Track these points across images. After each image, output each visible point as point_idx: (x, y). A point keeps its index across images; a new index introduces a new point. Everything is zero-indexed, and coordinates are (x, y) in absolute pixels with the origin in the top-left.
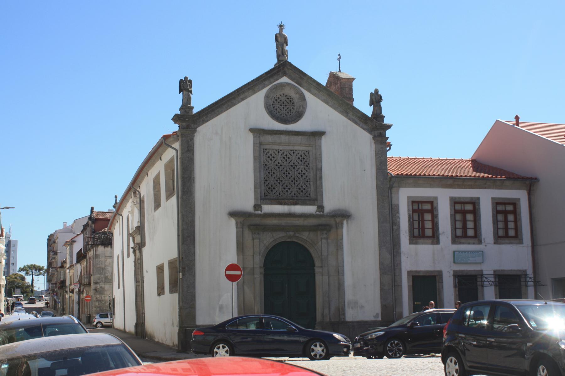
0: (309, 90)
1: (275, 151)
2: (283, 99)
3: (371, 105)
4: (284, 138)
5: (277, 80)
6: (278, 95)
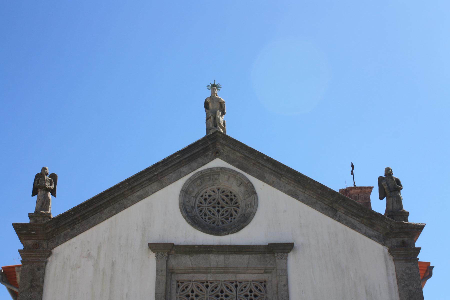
1: (200, 285)
2: (218, 196)
3: (381, 198)
4: (215, 260)
5: (204, 164)
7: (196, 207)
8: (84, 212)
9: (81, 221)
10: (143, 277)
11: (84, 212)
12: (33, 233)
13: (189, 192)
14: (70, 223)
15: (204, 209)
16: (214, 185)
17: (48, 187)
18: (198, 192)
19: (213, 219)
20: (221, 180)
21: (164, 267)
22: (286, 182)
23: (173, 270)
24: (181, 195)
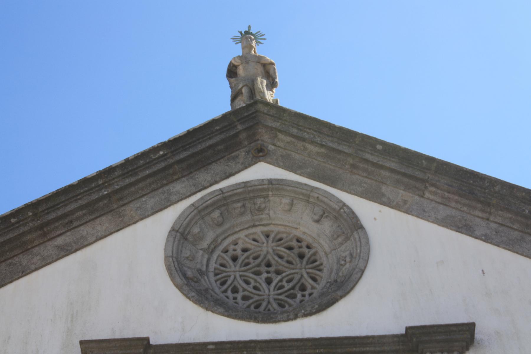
0: (374, 195)
2: (267, 248)
6: (243, 238)
7: (211, 275)
13: (190, 238)
15: (232, 278)
16: (254, 226)
18: (215, 240)
19: (256, 298)
20: (271, 213)
22: (439, 200)
24: (171, 239)
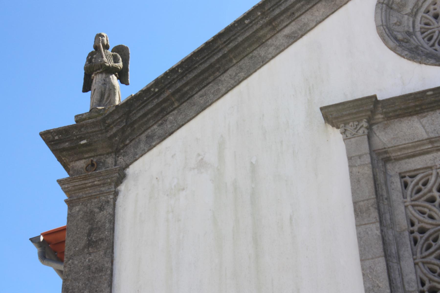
7: (418, 34)
8: (179, 85)
9: (176, 104)
10: (322, 184)
11: (179, 85)
12: (83, 142)
13: (394, 6)
14: (155, 112)
17: (110, 63)
21: (365, 148)
23: (386, 152)
24: (379, 11)
